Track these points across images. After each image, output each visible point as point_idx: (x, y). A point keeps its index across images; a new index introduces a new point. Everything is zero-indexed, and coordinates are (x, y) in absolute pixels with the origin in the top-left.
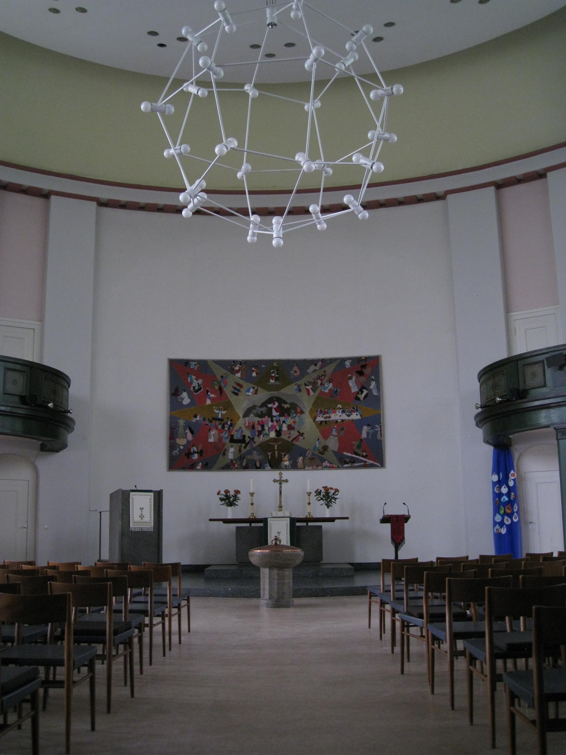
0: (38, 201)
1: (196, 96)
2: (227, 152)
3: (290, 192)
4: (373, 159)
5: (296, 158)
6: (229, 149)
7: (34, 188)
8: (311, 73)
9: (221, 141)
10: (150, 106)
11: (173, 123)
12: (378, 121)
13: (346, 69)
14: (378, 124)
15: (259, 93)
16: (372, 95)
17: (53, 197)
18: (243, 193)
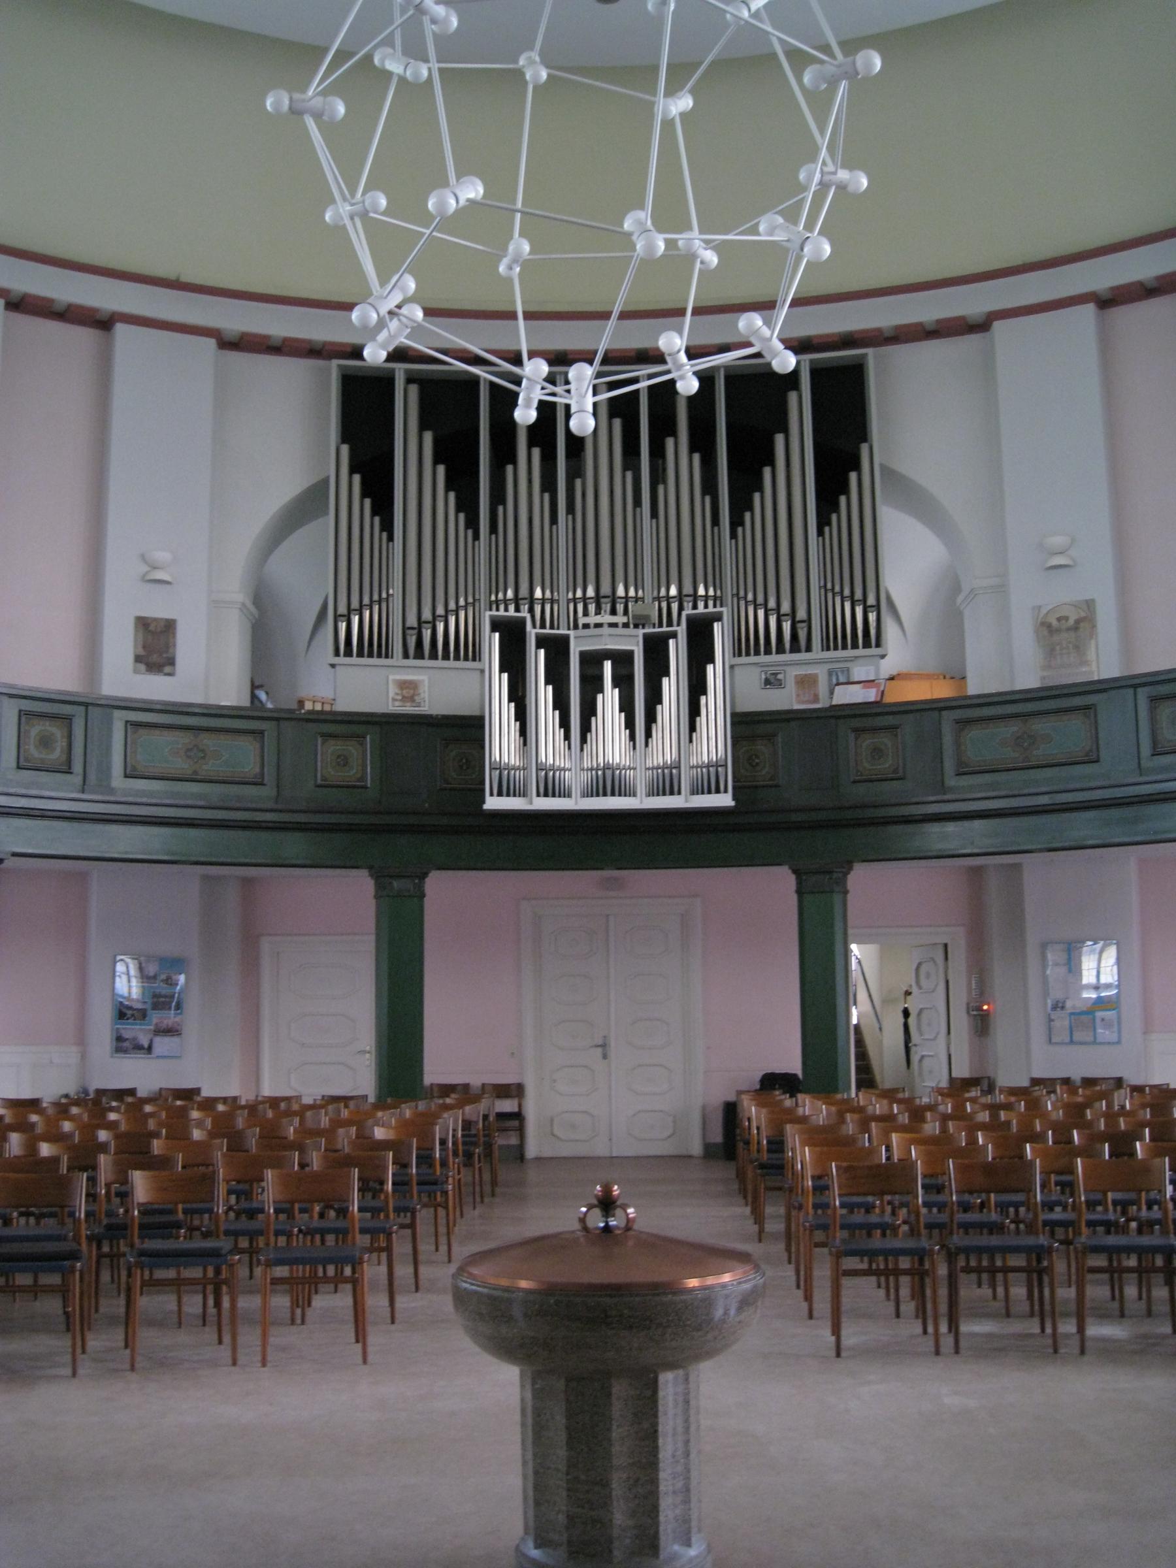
0: (84, 336)
1: (402, 80)
2: (457, 211)
3: (606, 316)
4: (809, 226)
5: (626, 226)
6: (462, 202)
7: (905, 326)
8: (660, 19)
9: (445, 184)
10: (286, 102)
11: (347, 141)
12: (822, 132)
13: (751, 16)
14: (824, 144)
15: (549, 75)
16: (807, 79)
17: (120, 328)
18: (512, 316)
